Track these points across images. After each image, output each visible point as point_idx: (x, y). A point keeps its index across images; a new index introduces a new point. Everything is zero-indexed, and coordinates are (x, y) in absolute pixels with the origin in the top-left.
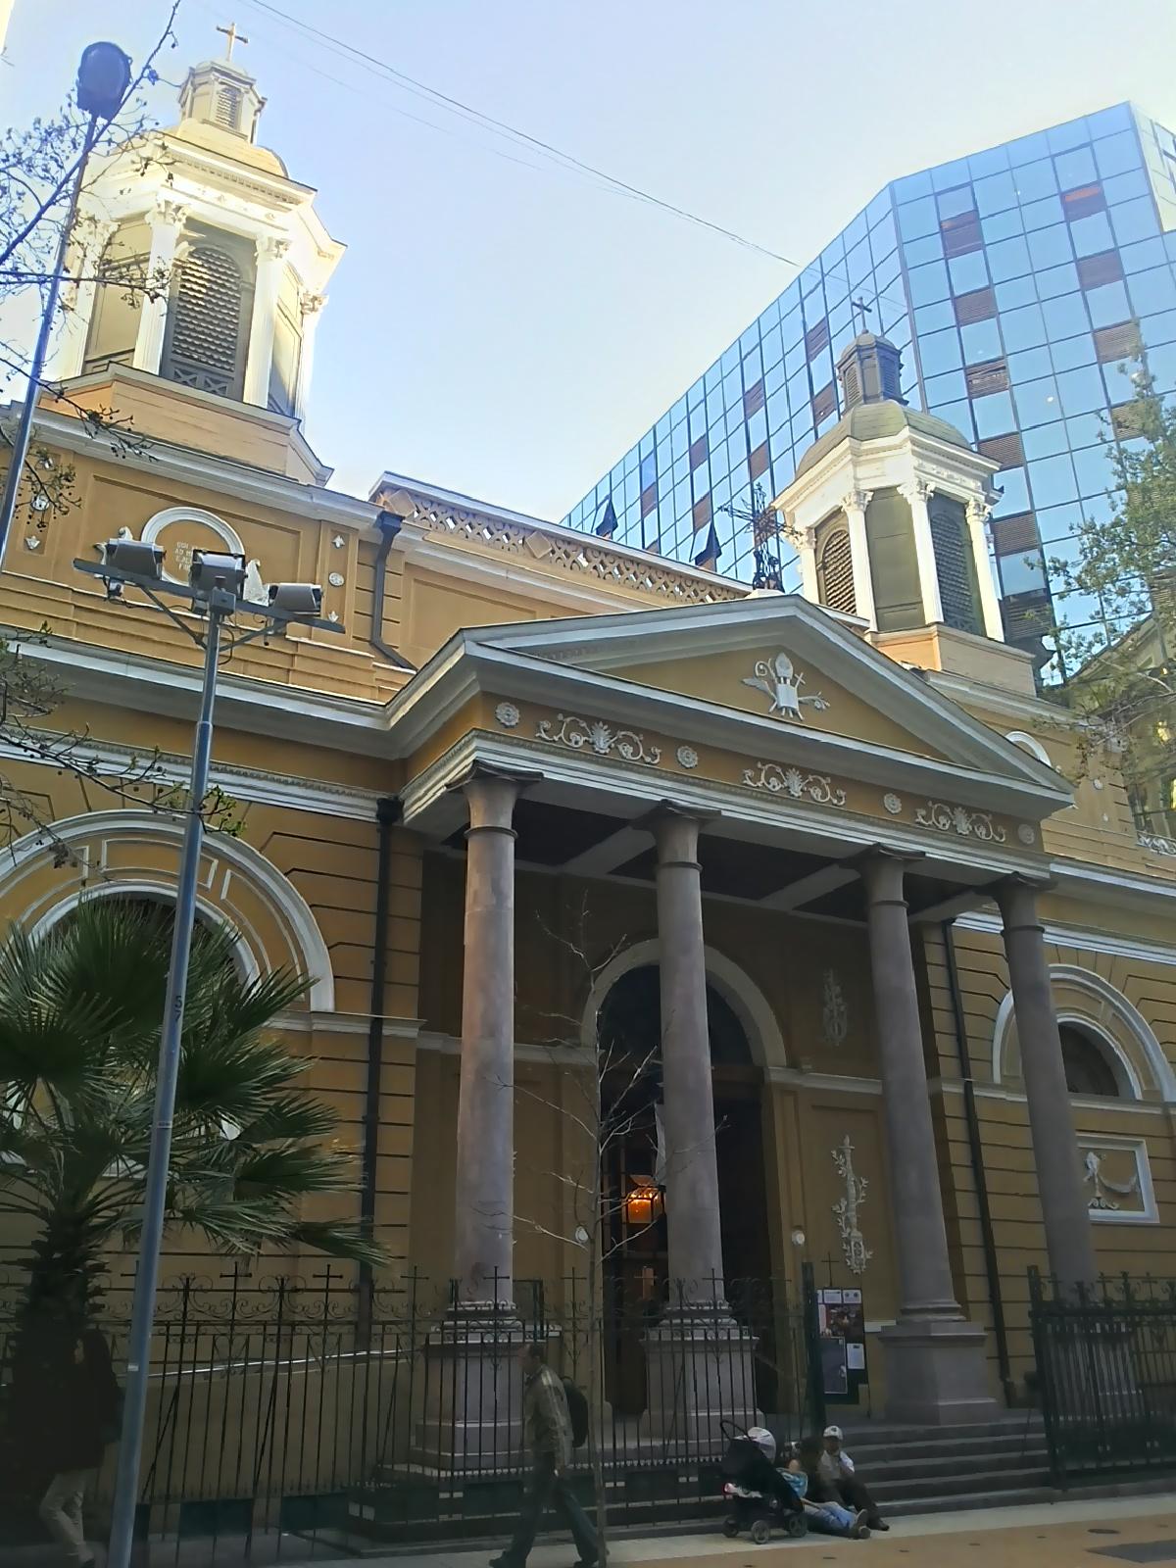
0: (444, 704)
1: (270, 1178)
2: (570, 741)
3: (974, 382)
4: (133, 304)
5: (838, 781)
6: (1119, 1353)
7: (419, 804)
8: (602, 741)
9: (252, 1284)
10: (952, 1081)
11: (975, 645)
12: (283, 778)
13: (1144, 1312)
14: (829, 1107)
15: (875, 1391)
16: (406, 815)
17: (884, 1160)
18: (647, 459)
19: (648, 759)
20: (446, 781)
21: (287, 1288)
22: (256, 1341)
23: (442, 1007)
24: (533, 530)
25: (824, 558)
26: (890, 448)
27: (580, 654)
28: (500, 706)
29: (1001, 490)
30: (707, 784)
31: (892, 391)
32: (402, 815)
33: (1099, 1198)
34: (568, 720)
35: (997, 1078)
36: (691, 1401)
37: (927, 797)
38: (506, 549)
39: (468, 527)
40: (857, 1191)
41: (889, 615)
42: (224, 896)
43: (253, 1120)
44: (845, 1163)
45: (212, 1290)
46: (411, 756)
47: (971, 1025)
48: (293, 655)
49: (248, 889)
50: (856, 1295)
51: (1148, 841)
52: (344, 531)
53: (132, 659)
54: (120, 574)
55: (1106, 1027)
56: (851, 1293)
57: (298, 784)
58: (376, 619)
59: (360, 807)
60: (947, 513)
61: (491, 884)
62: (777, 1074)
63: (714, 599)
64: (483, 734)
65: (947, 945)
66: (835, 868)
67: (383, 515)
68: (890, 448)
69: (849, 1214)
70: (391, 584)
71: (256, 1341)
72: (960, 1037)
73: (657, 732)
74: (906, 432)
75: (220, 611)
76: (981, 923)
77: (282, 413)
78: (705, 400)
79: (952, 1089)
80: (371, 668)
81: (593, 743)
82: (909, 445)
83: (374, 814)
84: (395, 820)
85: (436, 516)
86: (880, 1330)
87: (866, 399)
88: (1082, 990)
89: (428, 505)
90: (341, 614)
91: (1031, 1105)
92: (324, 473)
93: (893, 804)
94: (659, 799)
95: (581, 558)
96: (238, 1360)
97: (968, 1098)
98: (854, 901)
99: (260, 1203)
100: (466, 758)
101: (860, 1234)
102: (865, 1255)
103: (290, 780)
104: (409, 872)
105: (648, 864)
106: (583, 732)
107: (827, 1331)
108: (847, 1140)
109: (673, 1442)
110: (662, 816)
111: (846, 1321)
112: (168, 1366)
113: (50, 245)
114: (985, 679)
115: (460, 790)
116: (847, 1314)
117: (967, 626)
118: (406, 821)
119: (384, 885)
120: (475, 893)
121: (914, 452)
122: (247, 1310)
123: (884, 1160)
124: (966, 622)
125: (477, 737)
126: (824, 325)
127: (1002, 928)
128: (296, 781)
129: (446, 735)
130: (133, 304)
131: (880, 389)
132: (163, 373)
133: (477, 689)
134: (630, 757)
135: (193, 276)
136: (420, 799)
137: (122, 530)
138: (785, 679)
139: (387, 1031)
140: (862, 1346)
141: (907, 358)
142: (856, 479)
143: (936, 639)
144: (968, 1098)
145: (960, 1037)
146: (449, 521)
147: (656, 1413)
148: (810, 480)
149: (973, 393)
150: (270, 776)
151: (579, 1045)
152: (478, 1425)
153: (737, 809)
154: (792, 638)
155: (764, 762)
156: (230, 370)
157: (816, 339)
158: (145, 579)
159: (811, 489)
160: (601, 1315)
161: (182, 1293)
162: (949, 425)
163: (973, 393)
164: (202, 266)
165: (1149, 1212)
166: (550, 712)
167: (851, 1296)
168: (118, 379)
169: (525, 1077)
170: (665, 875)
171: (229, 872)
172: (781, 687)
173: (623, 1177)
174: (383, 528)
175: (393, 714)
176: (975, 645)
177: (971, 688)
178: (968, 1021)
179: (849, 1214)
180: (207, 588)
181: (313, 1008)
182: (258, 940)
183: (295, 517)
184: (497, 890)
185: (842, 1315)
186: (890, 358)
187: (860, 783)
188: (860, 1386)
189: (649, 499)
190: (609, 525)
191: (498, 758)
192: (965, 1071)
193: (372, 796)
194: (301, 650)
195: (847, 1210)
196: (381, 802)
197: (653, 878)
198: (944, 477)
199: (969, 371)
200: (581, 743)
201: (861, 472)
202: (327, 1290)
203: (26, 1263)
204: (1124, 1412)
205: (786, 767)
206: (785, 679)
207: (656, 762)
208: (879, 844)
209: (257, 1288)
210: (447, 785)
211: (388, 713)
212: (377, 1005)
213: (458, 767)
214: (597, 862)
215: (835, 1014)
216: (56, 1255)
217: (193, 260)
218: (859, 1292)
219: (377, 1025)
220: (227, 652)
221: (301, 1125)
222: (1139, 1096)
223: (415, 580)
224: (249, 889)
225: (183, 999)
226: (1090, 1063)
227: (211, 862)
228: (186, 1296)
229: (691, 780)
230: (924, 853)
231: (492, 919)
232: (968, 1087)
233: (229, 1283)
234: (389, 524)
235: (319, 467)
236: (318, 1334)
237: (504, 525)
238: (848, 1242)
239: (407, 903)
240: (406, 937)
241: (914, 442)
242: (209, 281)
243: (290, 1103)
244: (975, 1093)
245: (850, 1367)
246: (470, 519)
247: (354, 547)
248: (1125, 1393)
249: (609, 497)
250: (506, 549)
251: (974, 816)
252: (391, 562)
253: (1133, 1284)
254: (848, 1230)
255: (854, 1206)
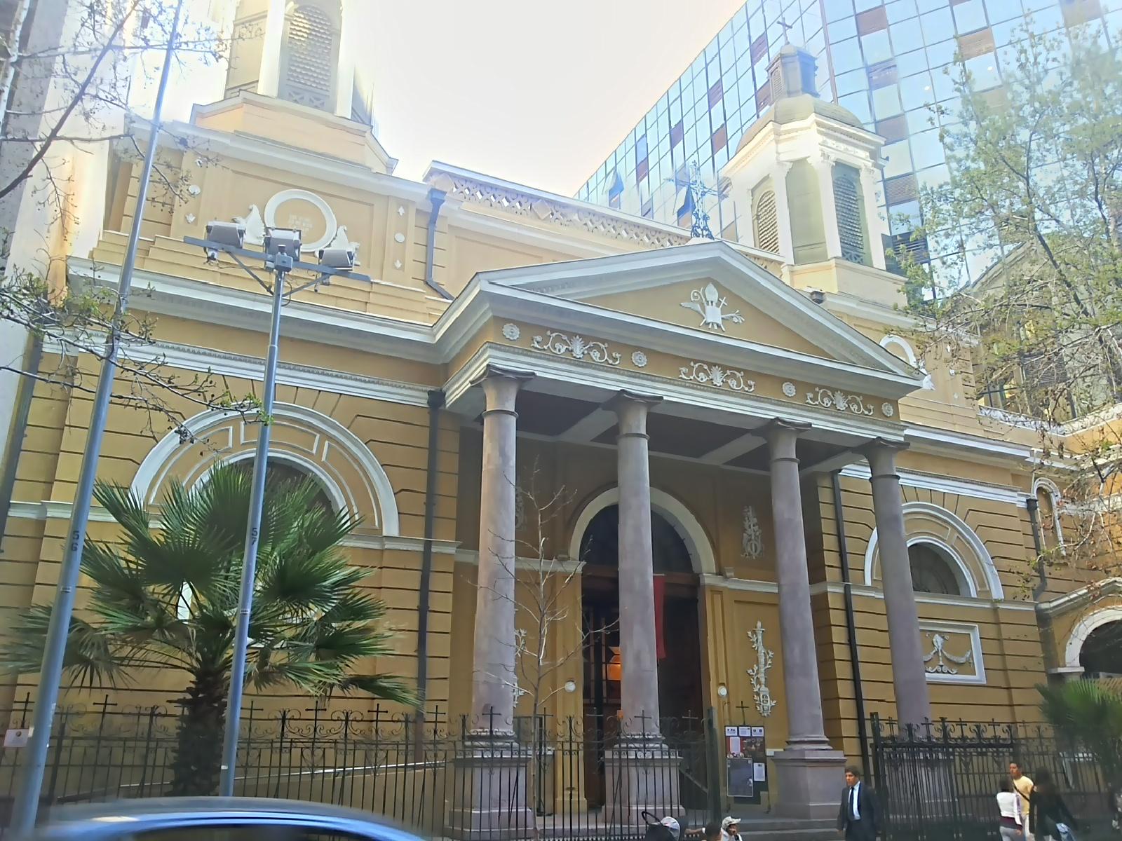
0: (470, 325)
1: (334, 646)
2: (555, 349)
3: (874, 78)
4: (206, 63)
5: (748, 374)
6: (651, 777)
7: (457, 392)
8: (578, 349)
9: (327, 715)
10: (834, 584)
11: (863, 273)
12: (363, 378)
13: (956, 746)
14: (744, 601)
15: (771, 796)
16: (447, 401)
17: (780, 638)
18: (640, 142)
19: (747, 389)
20: (471, 379)
21: (350, 718)
22: (330, 753)
23: (468, 535)
24: (538, 198)
25: (758, 212)
26: (802, 129)
27: (563, 288)
28: (508, 325)
29: (887, 159)
30: (653, 378)
31: (808, 87)
32: (445, 401)
33: (942, 666)
34: (554, 335)
35: (868, 582)
36: (633, 799)
37: (813, 385)
38: (519, 213)
39: (492, 198)
40: (766, 660)
41: (801, 252)
42: (323, 459)
43: (330, 608)
44: (757, 640)
45: (299, 719)
46: (451, 361)
47: (850, 545)
48: (369, 292)
49: (341, 457)
50: (760, 731)
51: (987, 412)
52: (405, 203)
53: (257, 297)
54: (214, 245)
55: (952, 547)
56: (758, 729)
57: (373, 382)
58: (428, 265)
59: (416, 397)
60: (846, 179)
61: (500, 447)
62: (709, 579)
63: (672, 244)
64: (494, 345)
65: (835, 490)
66: (748, 436)
67: (433, 191)
68: (802, 129)
69: (759, 676)
70: (438, 239)
71: (330, 753)
72: (842, 553)
73: (619, 343)
74: (813, 117)
75: (282, 269)
76: (857, 472)
77: (363, 123)
78: (681, 96)
79: (834, 591)
80: (425, 301)
81: (572, 351)
82: (815, 127)
83: (426, 402)
84: (440, 406)
85: (469, 190)
86: (773, 754)
87: (790, 94)
88: (934, 520)
89: (463, 183)
90: (403, 262)
91: (886, 600)
92: (390, 164)
93: (790, 390)
94: (619, 389)
95: (575, 217)
96: (318, 767)
97: (847, 598)
98: (762, 459)
99: (329, 662)
100: (482, 363)
101: (767, 689)
102: (770, 703)
103: (367, 379)
104: (450, 442)
105: (613, 435)
106: (565, 342)
107: (741, 754)
108: (759, 624)
109: (608, 826)
110: (621, 401)
111: (753, 748)
112: (282, 769)
113: (169, 18)
114: (870, 298)
115: (479, 386)
116: (755, 744)
117: (859, 259)
118: (448, 406)
119: (433, 450)
120: (489, 456)
121: (820, 132)
122: (324, 732)
123: (780, 638)
124: (859, 256)
125: (490, 347)
126: (763, 39)
127: (870, 475)
128: (371, 380)
129: (470, 347)
130: (206, 63)
131: (800, 86)
132: (280, 96)
133: (490, 315)
134: (735, 388)
135: (298, 26)
136: (457, 389)
137: (250, 207)
138: (712, 302)
139: (434, 549)
140: (763, 765)
141: (822, 62)
142: (778, 153)
143: (834, 269)
144: (847, 598)
145: (842, 553)
146: (478, 194)
147: (609, 806)
148: (743, 157)
149: (873, 86)
150: (353, 377)
151: (569, 558)
152: (479, 812)
153: (672, 394)
154: (716, 274)
155: (696, 361)
156: (327, 90)
157: (758, 48)
158: (232, 248)
159: (744, 164)
160: (581, 740)
161: (281, 721)
162: (847, 111)
163: (873, 86)
164: (304, 18)
165: (979, 677)
166: (542, 329)
167: (758, 731)
168: (246, 101)
169: (525, 581)
170: (624, 443)
171: (327, 442)
172: (708, 308)
173: (604, 648)
174: (432, 200)
175: (438, 331)
176: (863, 273)
177: (858, 305)
178: (848, 542)
179: (759, 676)
180: (274, 253)
181: (385, 534)
182: (347, 488)
183: (363, 194)
184: (503, 454)
185: (750, 744)
186: (807, 64)
187: (764, 375)
188: (762, 793)
189: (642, 170)
190: (617, 188)
191: (505, 363)
192: (845, 576)
193: (424, 389)
194: (375, 288)
195: (757, 674)
196: (430, 393)
197: (615, 443)
198: (842, 149)
199: (870, 70)
200: (563, 350)
201: (782, 147)
202: (436, 722)
203: (183, 702)
204: (937, 814)
205: (711, 365)
206: (712, 302)
207: (617, 363)
208: (777, 419)
209: (390, 719)
210: (471, 382)
211: (435, 331)
212: (428, 533)
213: (477, 370)
214: (584, 431)
215: (753, 538)
216: (200, 695)
217: (297, 15)
218: (762, 728)
219: (428, 545)
220: (287, 298)
221: (358, 612)
222: (974, 595)
223: (456, 237)
224: (341, 454)
225: (258, 530)
226: (934, 570)
227: (315, 436)
228: (347, 724)
229: (642, 376)
230: (810, 425)
231: (500, 474)
232: (847, 588)
233: (312, 715)
234: (437, 199)
235: (387, 158)
236: (92, 747)
237: (517, 195)
238: (758, 694)
239: (449, 463)
240: (448, 486)
241: (819, 124)
242: (309, 29)
243: (354, 597)
244: (852, 592)
245: (755, 780)
246: (494, 192)
247: (412, 212)
248: (945, 800)
249: (615, 168)
250: (519, 213)
251: (850, 397)
252: (439, 224)
253: (950, 727)
254: (758, 686)
255: (763, 670)
